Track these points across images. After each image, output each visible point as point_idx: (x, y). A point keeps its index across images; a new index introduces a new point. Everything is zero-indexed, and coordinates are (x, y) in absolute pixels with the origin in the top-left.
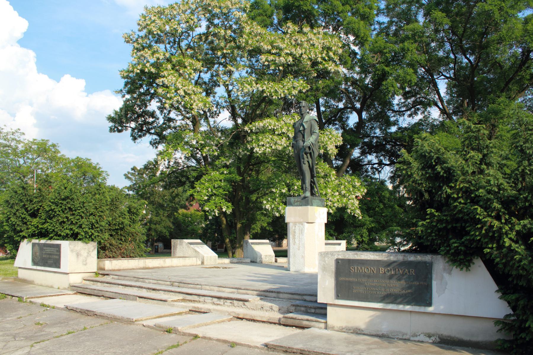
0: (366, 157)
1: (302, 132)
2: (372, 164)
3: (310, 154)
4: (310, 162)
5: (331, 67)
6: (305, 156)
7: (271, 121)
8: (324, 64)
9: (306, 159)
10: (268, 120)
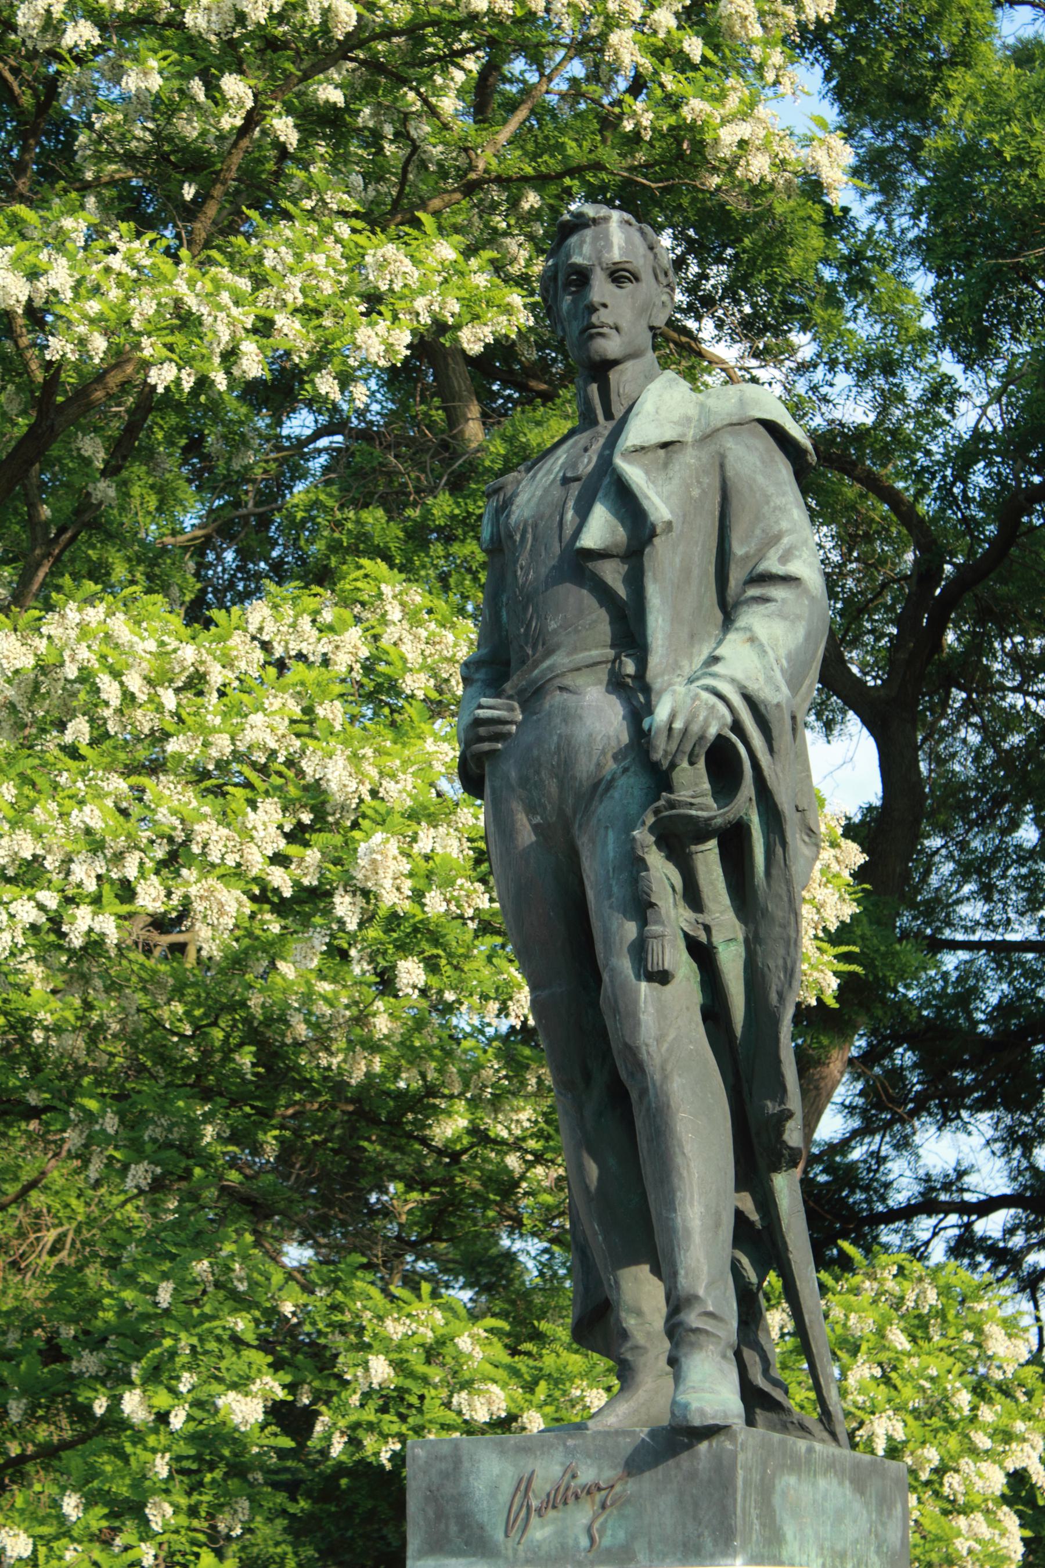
0: (903, 1144)
1: (612, 574)
2: (964, 1208)
3: (734, 842)
4: (731, 960)
5: (743, 130)
6: (661, 871)
7: (120, 626)
8: (673, 103)
9: (674, 916)
10: (94, 614)
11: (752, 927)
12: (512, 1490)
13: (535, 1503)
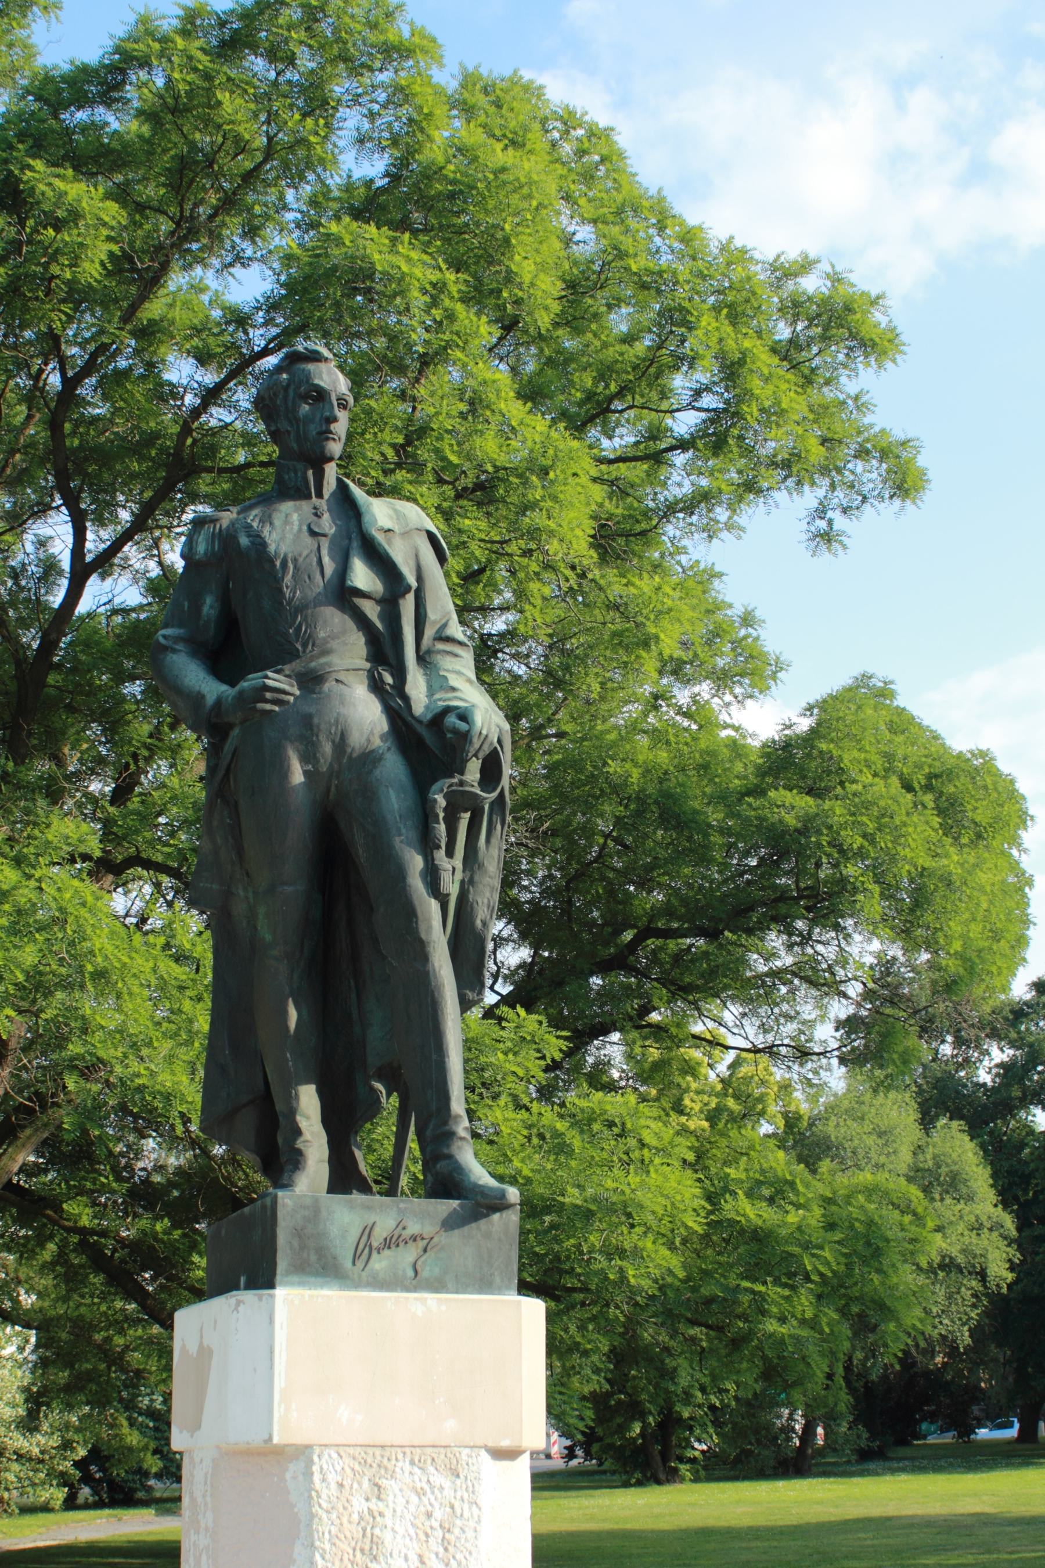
1: (371, 610)
11: (468, 873)
12: (358, 1235)
13: (375, 1244)
